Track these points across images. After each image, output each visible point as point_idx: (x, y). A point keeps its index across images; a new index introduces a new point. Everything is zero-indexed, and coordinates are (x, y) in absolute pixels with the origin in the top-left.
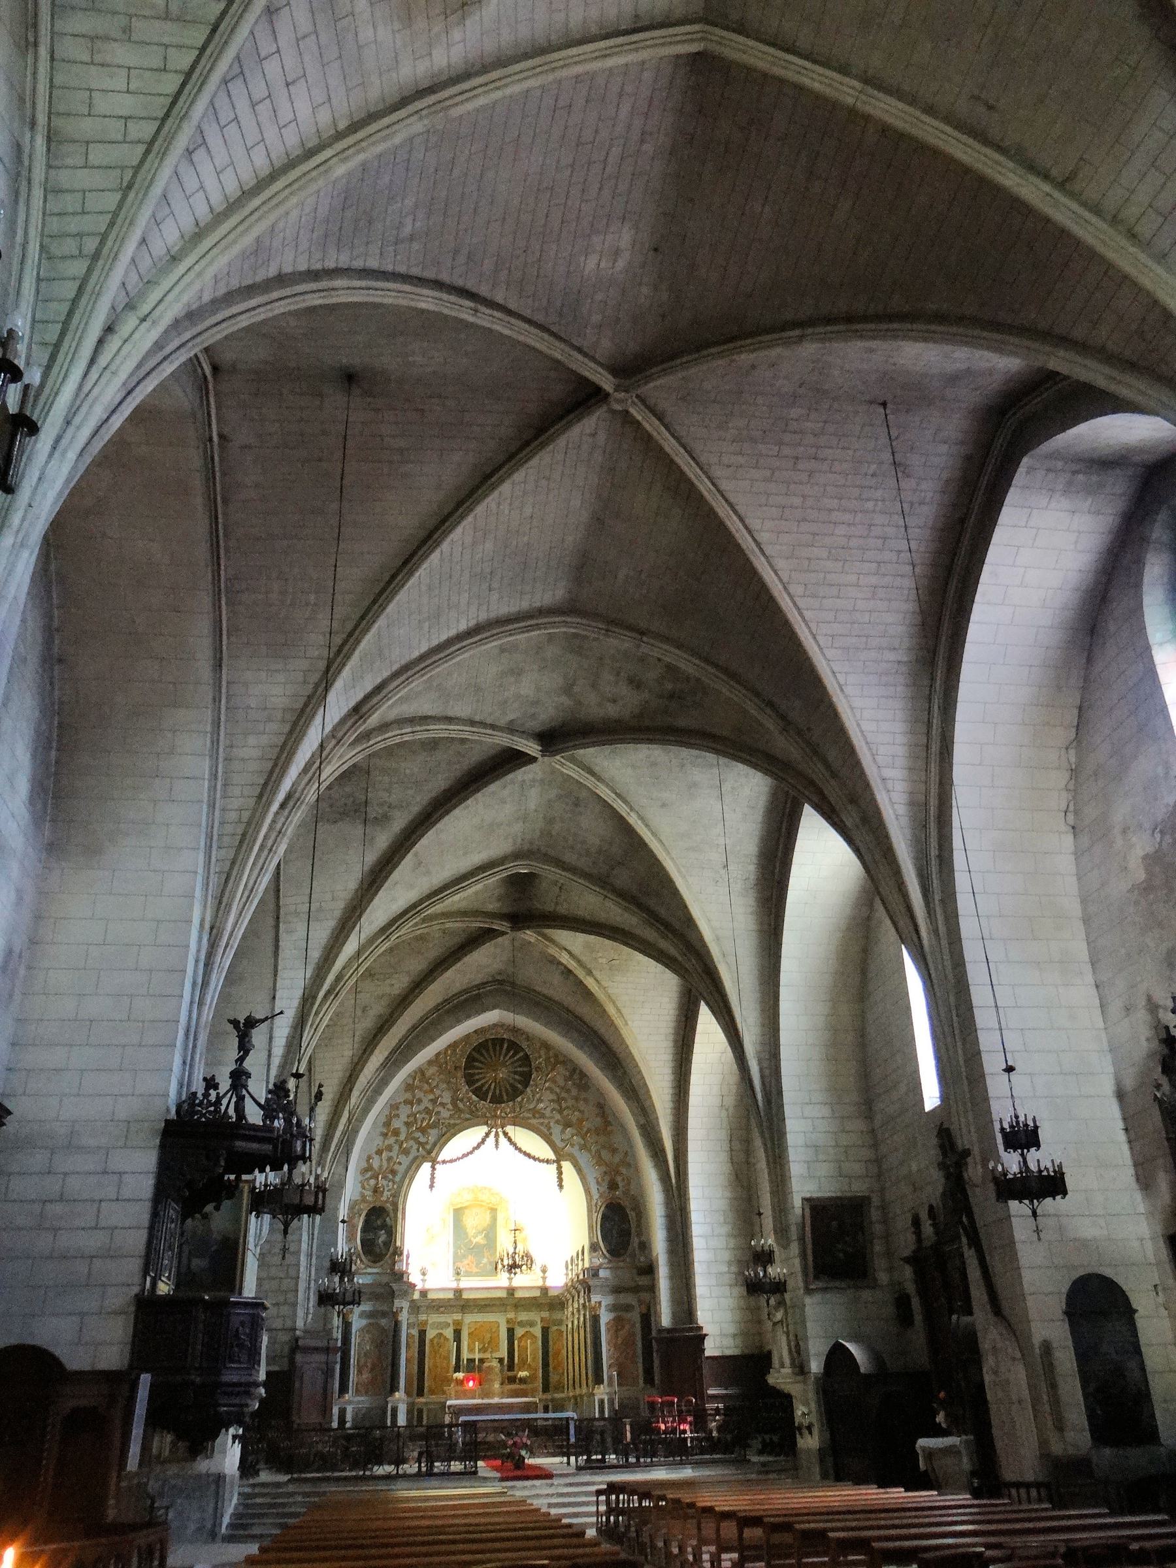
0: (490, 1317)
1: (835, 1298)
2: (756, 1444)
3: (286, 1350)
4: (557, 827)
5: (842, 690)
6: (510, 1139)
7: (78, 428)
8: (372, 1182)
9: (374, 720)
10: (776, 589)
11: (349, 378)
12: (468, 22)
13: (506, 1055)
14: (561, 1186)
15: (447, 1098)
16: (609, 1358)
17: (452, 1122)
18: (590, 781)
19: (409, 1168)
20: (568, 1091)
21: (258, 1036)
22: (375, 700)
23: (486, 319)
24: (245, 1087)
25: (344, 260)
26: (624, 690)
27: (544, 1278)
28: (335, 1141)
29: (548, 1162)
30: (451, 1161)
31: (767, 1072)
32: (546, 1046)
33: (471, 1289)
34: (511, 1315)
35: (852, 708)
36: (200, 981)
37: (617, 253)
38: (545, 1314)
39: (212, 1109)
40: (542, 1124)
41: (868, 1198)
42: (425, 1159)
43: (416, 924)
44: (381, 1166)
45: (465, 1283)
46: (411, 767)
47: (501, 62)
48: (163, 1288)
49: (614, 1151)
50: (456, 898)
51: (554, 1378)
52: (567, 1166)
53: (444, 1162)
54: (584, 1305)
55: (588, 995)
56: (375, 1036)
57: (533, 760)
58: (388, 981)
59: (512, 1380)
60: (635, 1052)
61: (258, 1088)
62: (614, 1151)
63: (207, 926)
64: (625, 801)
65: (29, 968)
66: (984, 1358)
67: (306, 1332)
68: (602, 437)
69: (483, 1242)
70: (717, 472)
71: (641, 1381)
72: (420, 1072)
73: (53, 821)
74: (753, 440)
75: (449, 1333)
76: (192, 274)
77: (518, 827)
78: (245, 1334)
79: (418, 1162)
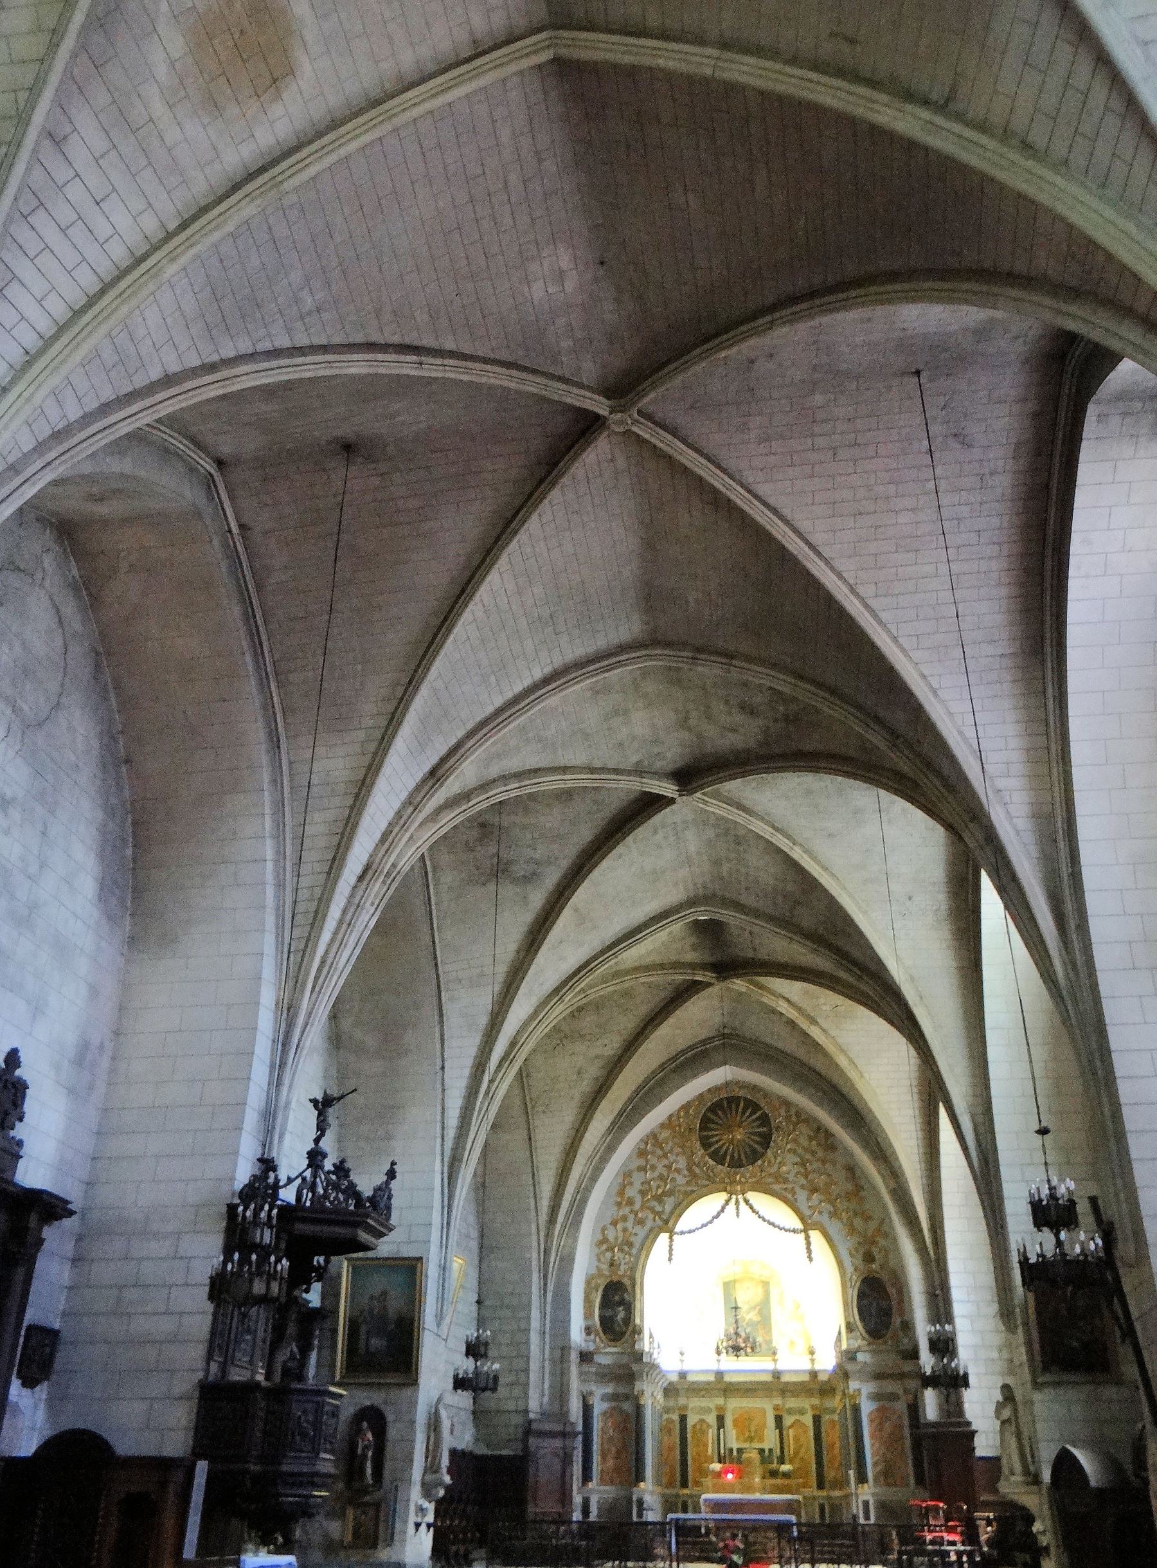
1: (1071, 1394)
3: (520, 1435)
4: (725, 867)
8: (608, 1255)
10: (840, 592)
11: (348, 448)
12: (285, 95)
13: (743, 1113)
14: (810, 1258)
15: (682, 1163)
17: (690, 1188)
18: (740, 818)
19: (647, 1237)
20: (813, 1153)
22: (452, 762)
23: (433, 369)
25: (245, 347)
26: (739, 718)
27: (813, 1361)
29: (794, 1231)
30: (690, 1232)
31: (982, 1129)
32: (787, 1103)
33: (735, 1371)
35: (950, 714)
37: (561, 276)
38: (816, 1401)
42: (661, 1230)
44: (616, 1238)
46: (552, 819)
47: (335, 124)
49: (867, 1219)
52: (816, 1236)
53: (682, 1233)
55: (817, 1046)
57: (672, 801)
58: (599, 1043)
59: (774, 1474)
62: (867, 1219)
64: (788, 836)
67: (543, 1414)
68: (621, 462)
70: (749, 477)
71: (912, 1481)
72: (653, 1136)
73: (132, 915)
74: (782, 437)
75: (711, 1419)
76: (22, 400)
77: (684, 872)
78: (307, 1421)
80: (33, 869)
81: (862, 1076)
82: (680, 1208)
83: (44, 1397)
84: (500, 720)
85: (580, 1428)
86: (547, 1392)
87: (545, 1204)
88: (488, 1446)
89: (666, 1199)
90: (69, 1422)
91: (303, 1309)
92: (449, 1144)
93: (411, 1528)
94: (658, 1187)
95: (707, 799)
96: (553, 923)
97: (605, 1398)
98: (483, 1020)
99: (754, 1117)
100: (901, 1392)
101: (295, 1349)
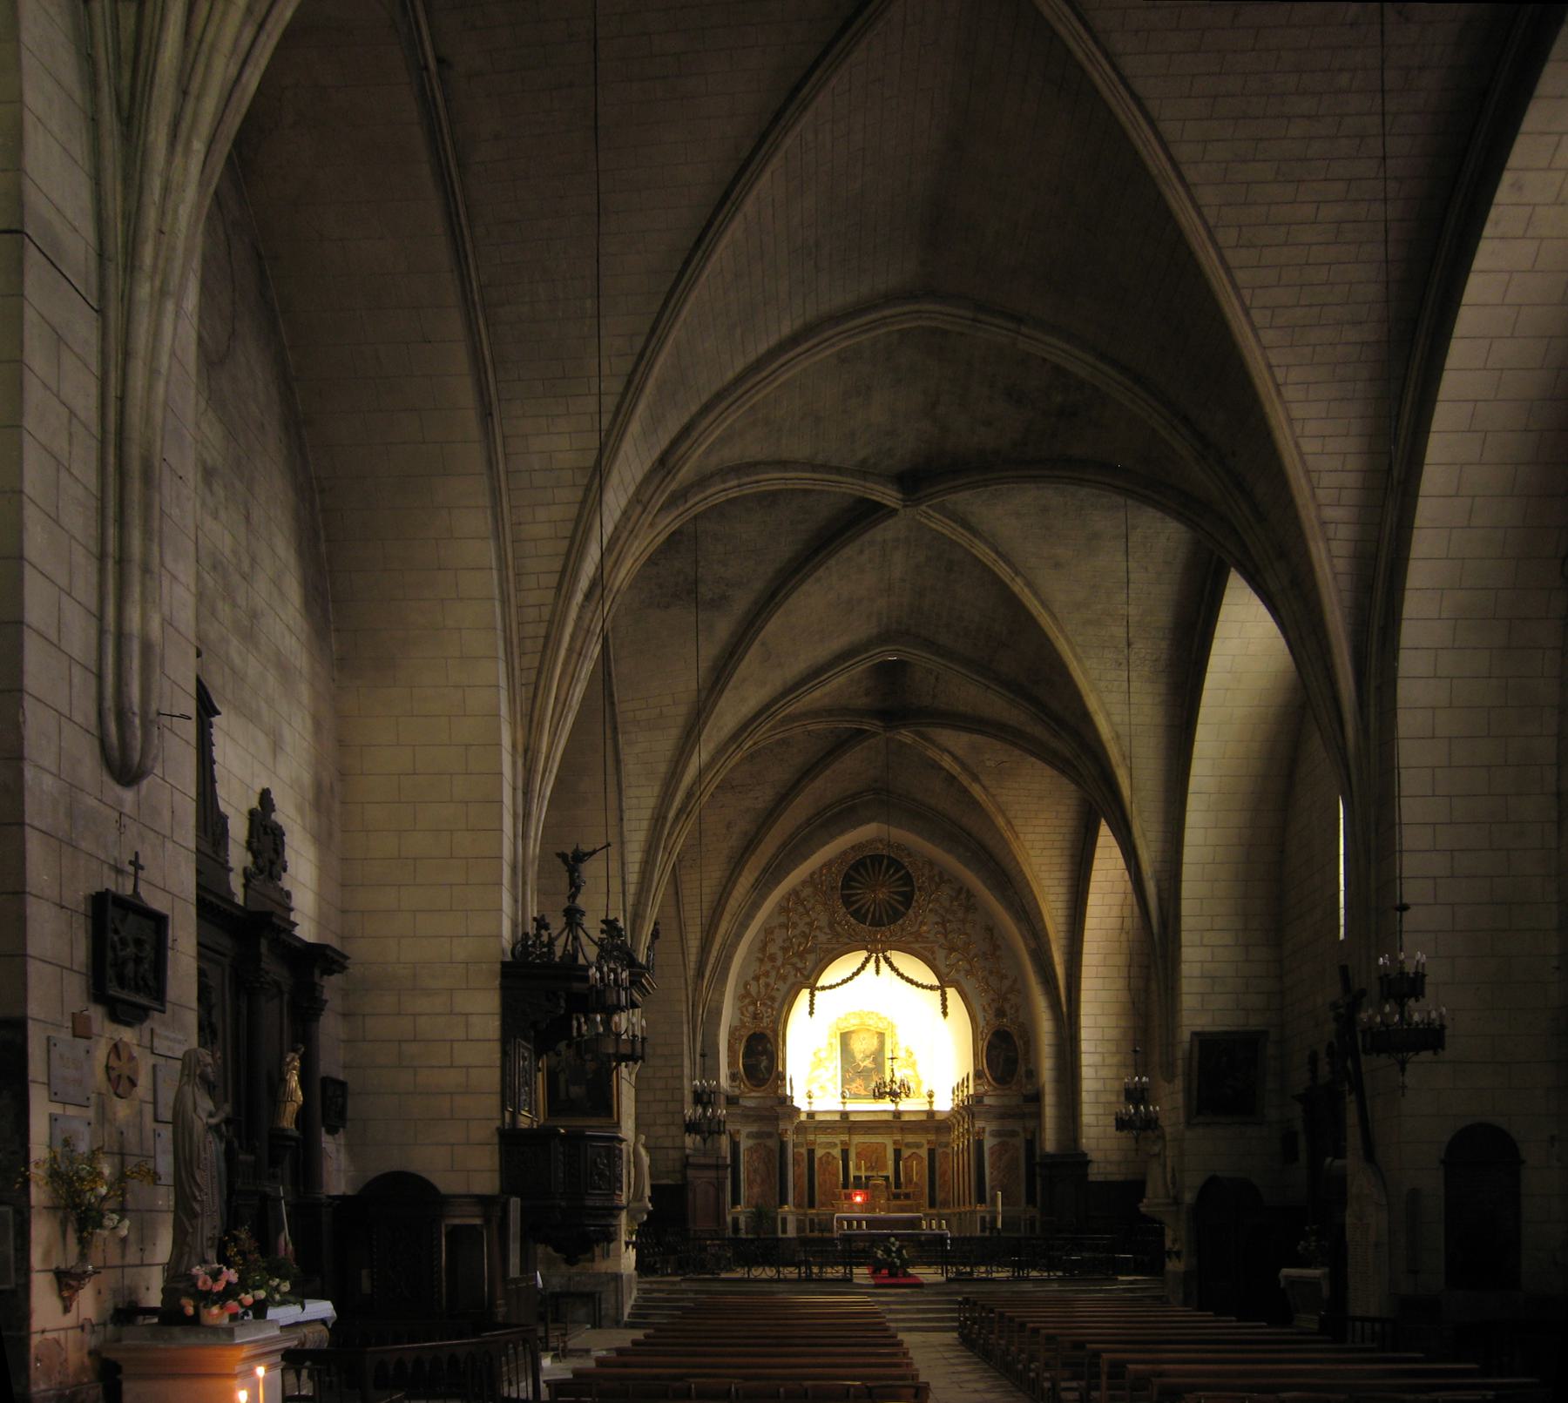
5: (1279, 393)
6: (891, 965)
7: (199, 98)
8: (751, 1008)
9: (686, 473)
14: (945, 1013)
15: (823, 920)
16: (992, 1180)
17: (830, 946)
19: (788, 992)
21: (592, 870)
24: (580, 925)
28: (709, 967)
29: (931, 988)
30: (831, 987)
32: (931, 863)
34: (898, 1137)
36: (520, 811)
38: (932, 1137)
39: (545, 950)
40: (924, 948)
43: (774, 728)
45: (851, 1106)
48: (524, 1121)
50: (817, 694)
51: (940, 1196)
52: (952, 993)
53: (823, 988)
54: (968, 1130)
55: (975, 804)
56: (742, 855)
59: (897, 1197)
60: (1026, 869)
61: (592, 925)
63: (520, 748)
65: (343, 803)
69: (871, 1066)
71: (1024, 1199)
72: (795, 893)
75: (837, 1152)
78: (603, 1164)
80: (246, 567)
81: (1017, 837)
83: (342, 1142)
84: (740, 391)
87: (692, 958)
90: (378, 1168)
92: (630, 900)
95: (931, 512)
96: (741, 659)
97: (749, 1136)
98: (662, 768)
99: (897, 876)
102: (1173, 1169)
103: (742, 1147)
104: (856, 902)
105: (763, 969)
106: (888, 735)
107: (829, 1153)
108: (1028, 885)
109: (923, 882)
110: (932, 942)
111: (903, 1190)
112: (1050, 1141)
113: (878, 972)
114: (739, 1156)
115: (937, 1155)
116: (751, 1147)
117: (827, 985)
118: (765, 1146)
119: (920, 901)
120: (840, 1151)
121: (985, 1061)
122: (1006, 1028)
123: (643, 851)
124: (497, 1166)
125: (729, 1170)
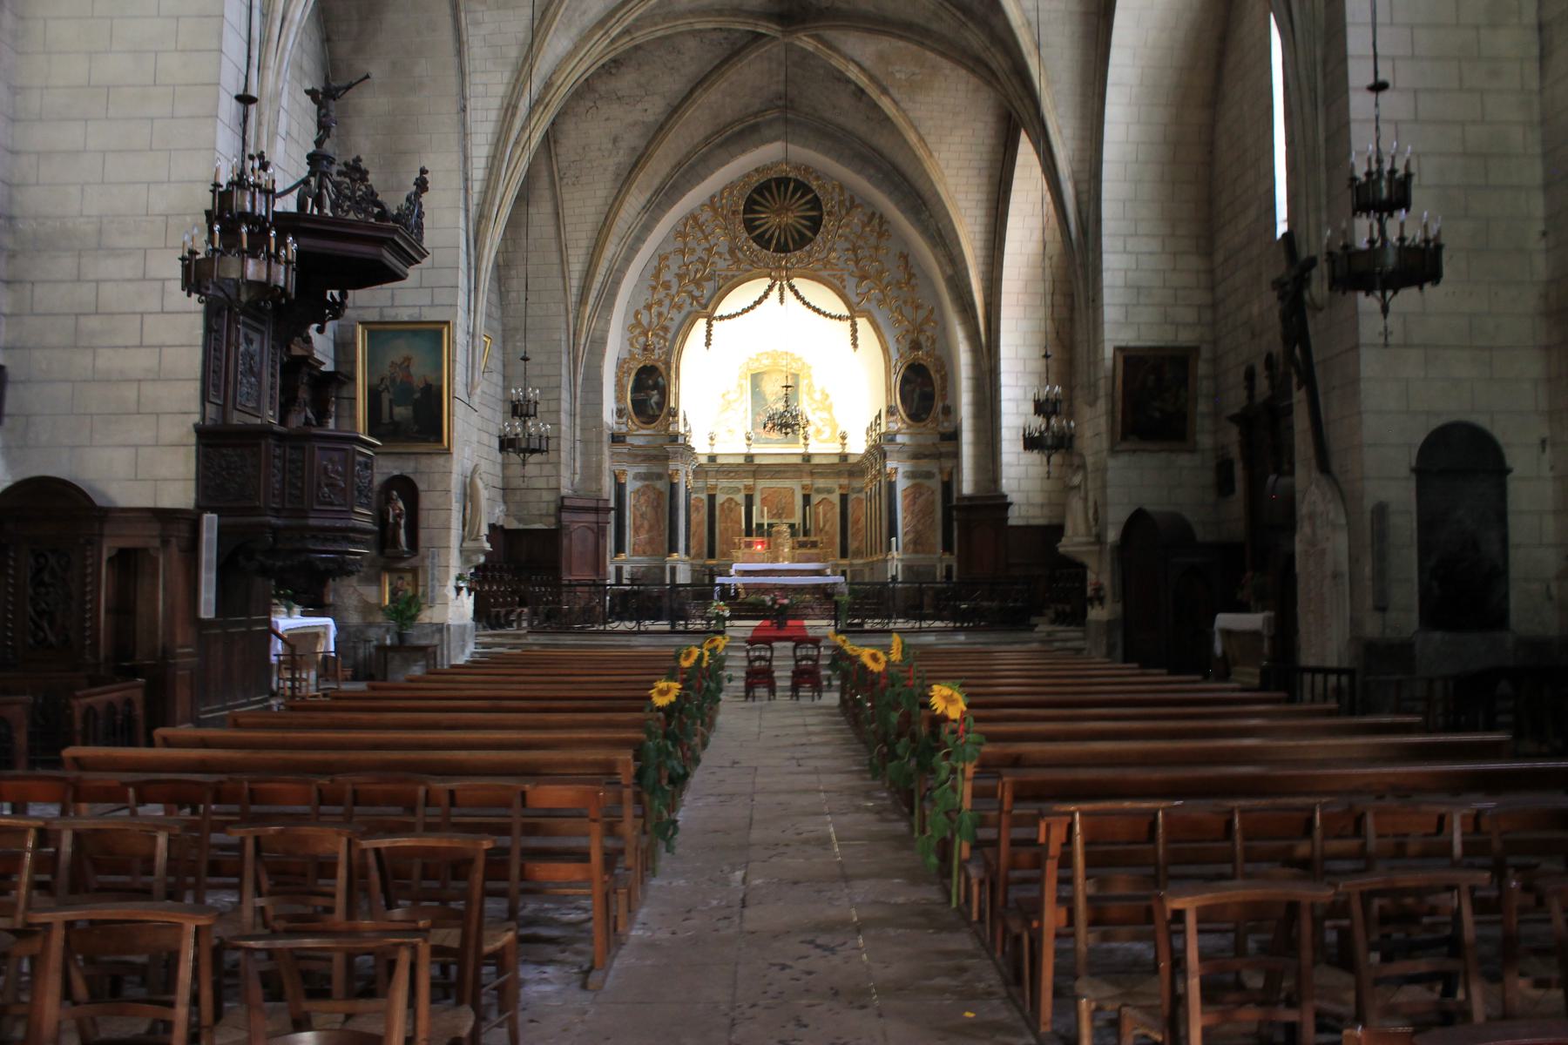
0: (788, 483)
2: (1051, 613)
6: (796, 293)
8: (642, 339)
14: (855, 345)
16: (905, 526)
17: (730, 273)
27: (844, 445)
29: (840, 318)
30: (730, 317)
31: (1084, 197)
34: (807, 481)
40: (834, 276)
41: (1196, 350)
51: (853, 545)
52: (863, 324)
53: (721, 318)
55: (886, 120)
56: (630, 173)
58: (639, 106)
59: (802, 545)
60: (941, 189)
62: (918, 307)
66: (1298, 526)
72: (692, 218)
78: (337, 472)
79: (691, 318)
81: (931, 155)
82: (721, 293)
85: (612, 504)
86: (578, 471)
87: (575, 283)
88: (520, 520)
89: (705, 283)
91: (315, 373)
93: (452, 593)
94: (696, 272)
97: (637, 477)
98: (514, 53)
100: (936, 471)
101: (310, 415)
102: (1096, 503)
103: (628, 489)
104: (760, 226)
105: (655, 297)
106: (786, 40)
107: (732, 499)
108: (944, 207)
109: (833, 207)
110: (842, 270)
111: (813, 538)
112: (967, 485)
113: (782, 300)
114: (624, 500)
115: (849, 501)
116: (638, 490)
117: (725, 314)
118: (654, 489)
119: (829, 227)
120: (743, 497)
121: (898, 396)
122: (922, 362)
123: (491, 145)
124: (193, 475)
125: (613, 512)
